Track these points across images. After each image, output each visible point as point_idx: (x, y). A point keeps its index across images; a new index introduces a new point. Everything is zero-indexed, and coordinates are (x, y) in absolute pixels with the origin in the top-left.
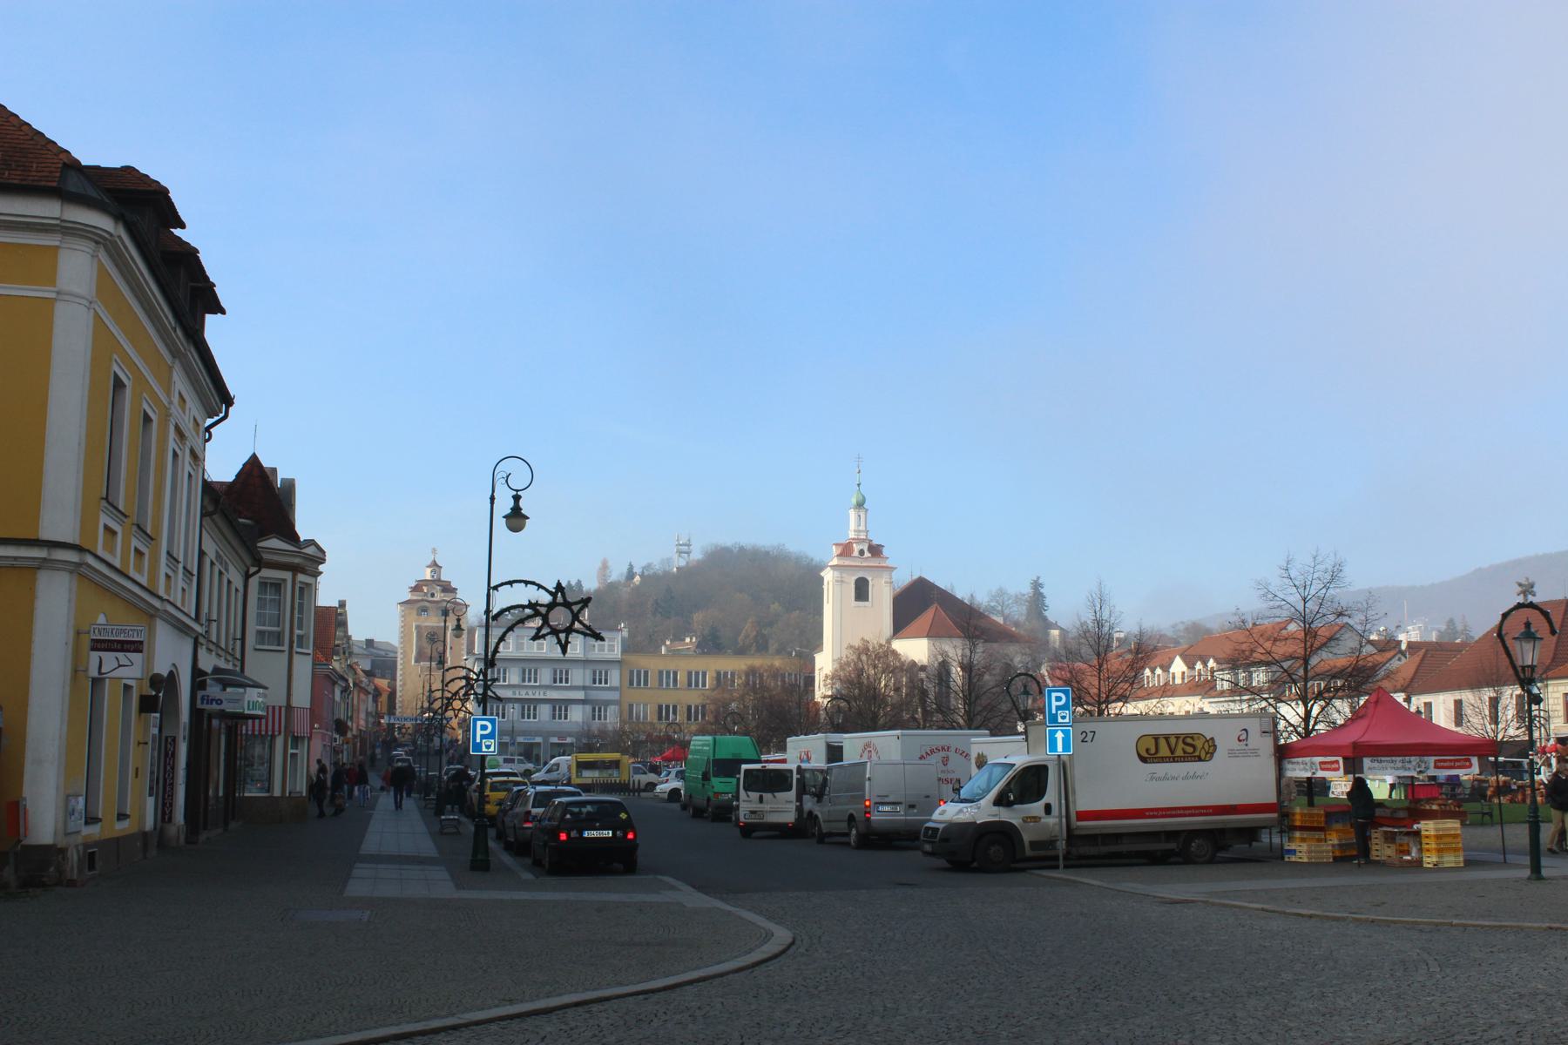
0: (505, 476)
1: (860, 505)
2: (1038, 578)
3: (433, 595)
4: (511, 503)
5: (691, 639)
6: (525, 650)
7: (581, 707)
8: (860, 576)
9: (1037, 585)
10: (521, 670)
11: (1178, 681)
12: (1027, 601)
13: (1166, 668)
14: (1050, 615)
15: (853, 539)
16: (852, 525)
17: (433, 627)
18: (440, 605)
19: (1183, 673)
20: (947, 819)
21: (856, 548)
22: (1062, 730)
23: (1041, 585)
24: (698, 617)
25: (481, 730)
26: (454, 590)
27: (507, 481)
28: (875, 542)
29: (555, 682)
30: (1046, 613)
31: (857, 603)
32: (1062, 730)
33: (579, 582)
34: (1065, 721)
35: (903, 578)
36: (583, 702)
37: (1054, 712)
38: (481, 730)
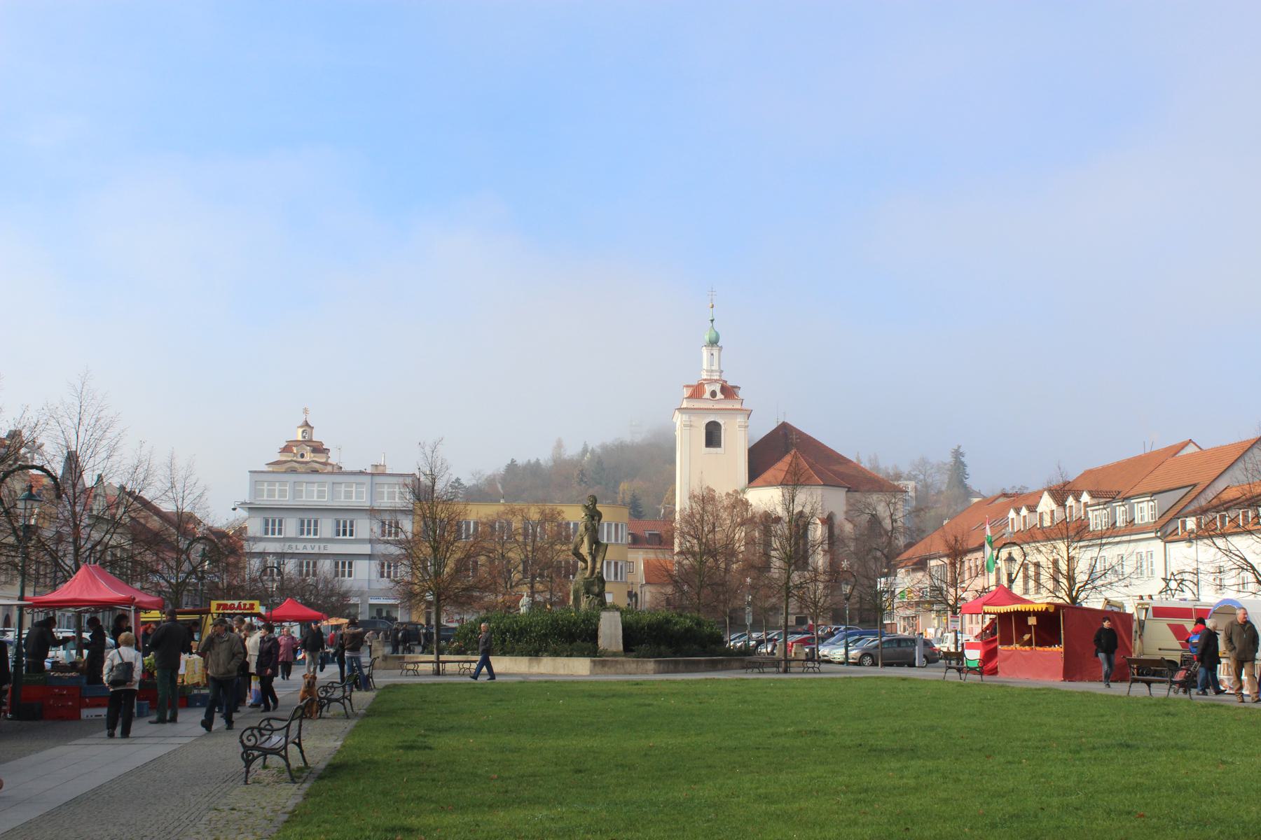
1: (713, 343)
2: (959, 447)
3: (302, 456)
6: (304, 499)
7: (367, 562)
8: (712, 420)
9: (958, 454)
10: (299, 523)
11: (1047, 523)
12: (948, 470)
13: (1032, 509)
14: (973, 482)
15: (705, 380)
18: (309, 466)
19: (1052, 512)
20: (145, 718)
21: (708, 389)
23: (962, 455)
24: (624, 486)
26: (326, 451)
28: (730, 383)
29: (266, 533)
30: (967, 482)
31: (708, 449)
35: (763, 427)
36: (370, 557)
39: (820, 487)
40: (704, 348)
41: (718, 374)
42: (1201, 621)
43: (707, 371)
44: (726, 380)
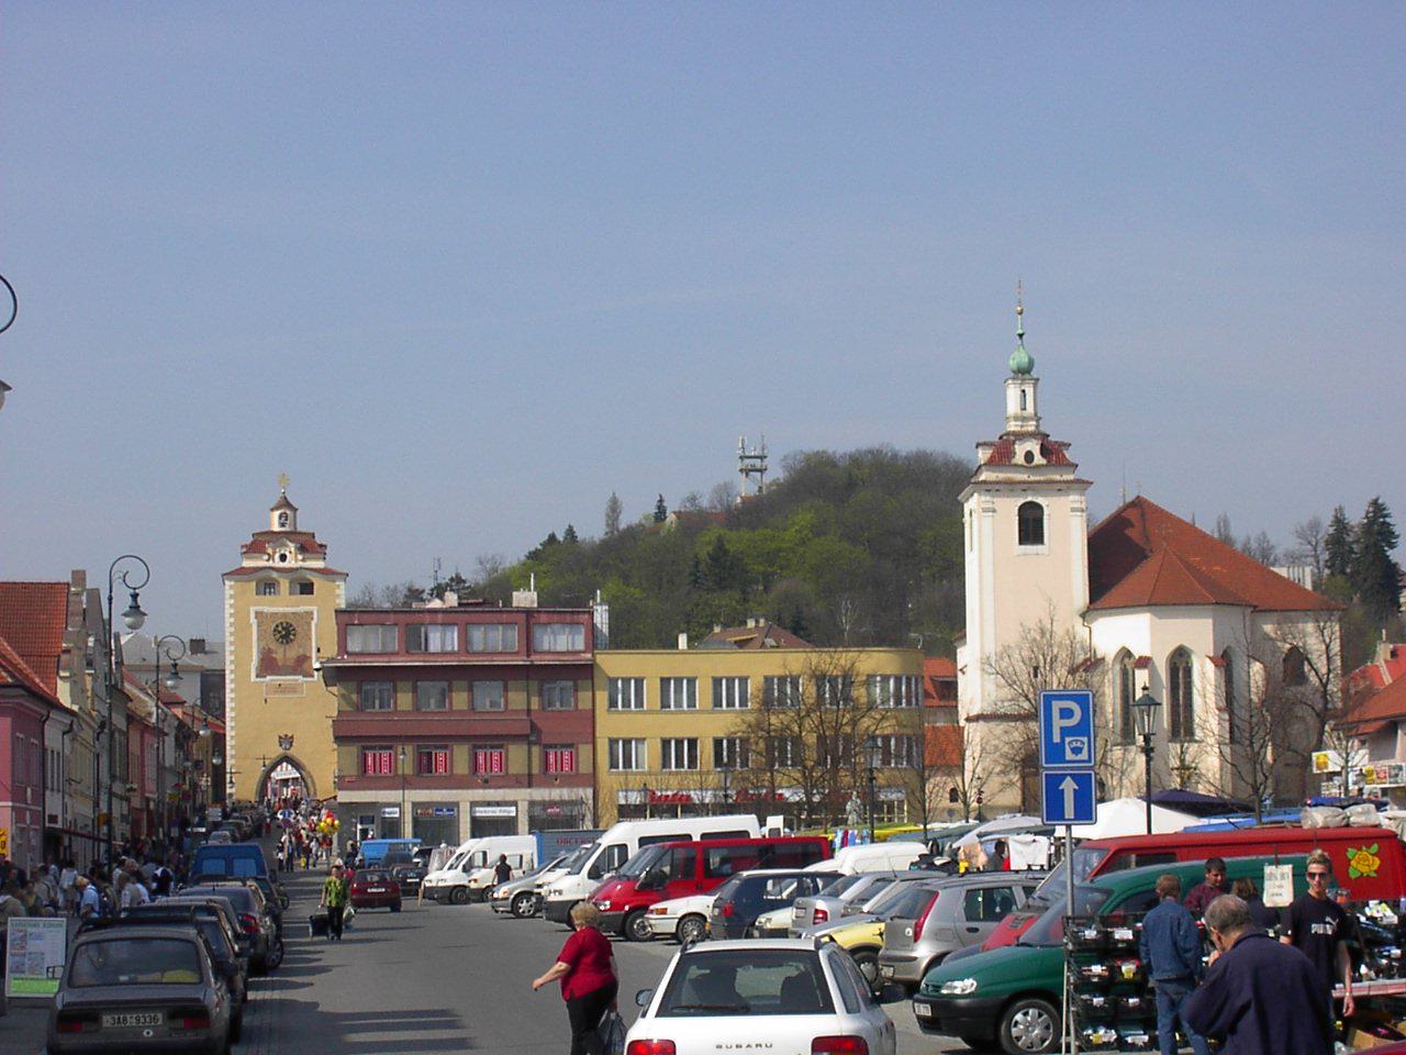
0: (122, 575)
3: (283, 558)
4: (129, 601)
5: (757, 622)
16: (1013, 406)
17: (285, 615)
21: (1020, 450)
22: (1070, 775)
25: (1061, 717)
27: (124, 581)
30: (1394, 555)
31: (1023, 547)
32: (1073, 777)
33: (570, 532)
34: (1079, 757)
37: (1057, 739)
38: (1061, 717)
39: (1211, 607)
40: (1010, 382)
41: (1034, 423)
42: (1052, 844)
43: (1016, 418)
44: (1048, 433)
